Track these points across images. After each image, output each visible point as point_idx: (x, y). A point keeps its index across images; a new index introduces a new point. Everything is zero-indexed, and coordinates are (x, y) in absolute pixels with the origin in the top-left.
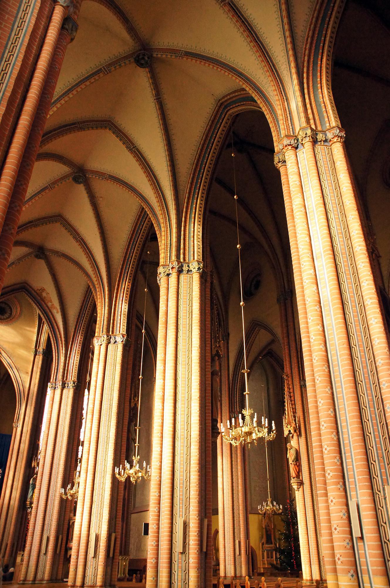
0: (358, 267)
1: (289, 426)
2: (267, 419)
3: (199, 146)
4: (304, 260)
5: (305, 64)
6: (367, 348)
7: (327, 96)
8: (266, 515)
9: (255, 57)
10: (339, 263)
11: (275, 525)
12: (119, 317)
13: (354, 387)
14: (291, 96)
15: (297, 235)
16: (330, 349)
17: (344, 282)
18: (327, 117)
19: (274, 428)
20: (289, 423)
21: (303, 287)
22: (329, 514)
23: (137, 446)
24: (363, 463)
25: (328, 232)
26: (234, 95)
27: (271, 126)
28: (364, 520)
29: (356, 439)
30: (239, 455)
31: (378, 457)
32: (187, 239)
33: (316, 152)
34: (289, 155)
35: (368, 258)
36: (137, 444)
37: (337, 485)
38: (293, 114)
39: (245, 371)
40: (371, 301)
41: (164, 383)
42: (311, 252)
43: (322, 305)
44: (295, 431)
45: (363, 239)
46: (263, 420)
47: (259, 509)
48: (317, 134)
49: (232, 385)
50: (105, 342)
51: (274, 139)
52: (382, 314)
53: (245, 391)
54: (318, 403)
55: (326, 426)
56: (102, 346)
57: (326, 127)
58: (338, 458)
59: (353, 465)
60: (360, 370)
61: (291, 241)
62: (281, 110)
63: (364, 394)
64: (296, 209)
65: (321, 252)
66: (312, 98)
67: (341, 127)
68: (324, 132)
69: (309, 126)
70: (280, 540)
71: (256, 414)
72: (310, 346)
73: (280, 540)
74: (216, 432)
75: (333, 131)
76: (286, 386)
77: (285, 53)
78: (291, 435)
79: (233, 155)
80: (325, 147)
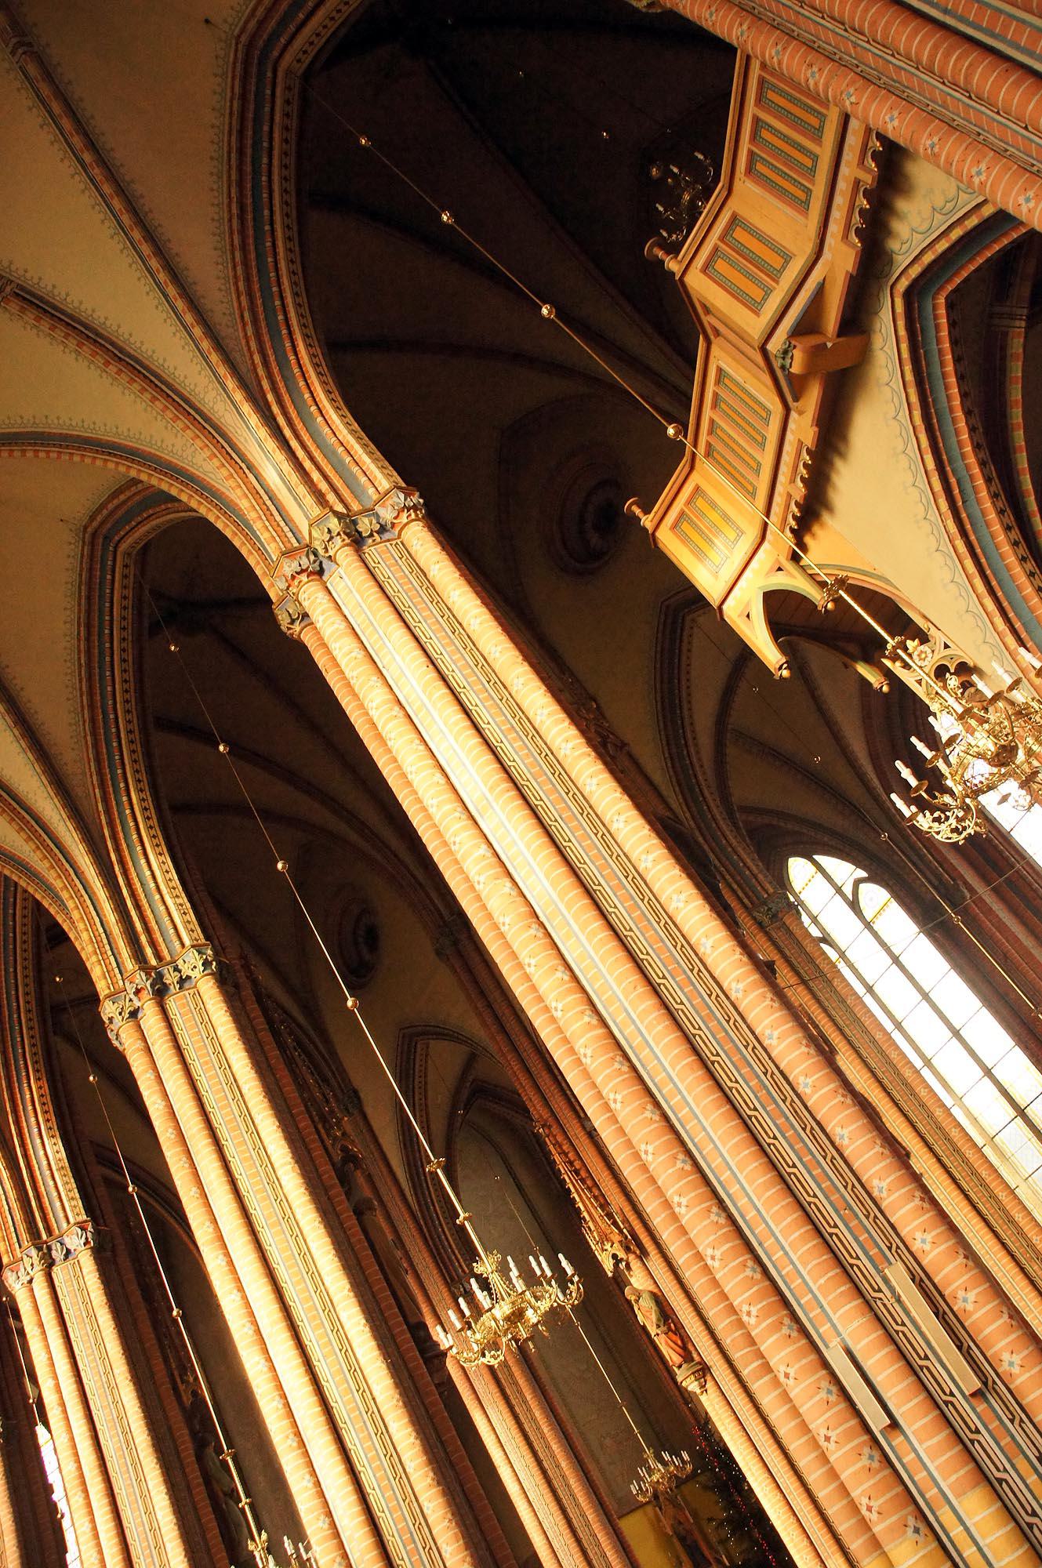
1: (608, 1246)
2: (542, 1259)
3: (79, 658)
5: (261, 371)
7: (341, 427)
8: (661, 1499)
9: (132, 396)
11: (695, 1515)
12: (51, 1183)
13: (707, 1077)
14: (257, 456)
15: (410, 777)
16: (609, 1014)
17: (570, 841)
19: (569, 1270)
20: (604, 1238)
21: (478, 898)
22: (795, 1412)
23: (247, 1507)
24: (810, 1245)
26: (116, 502)
27: (237, 543)
28: (878, 1380)
30: (521, 1381)
31: (837, 1211)
32: (144, 901)
33: (372, 564)
34: (311, 596)
36: (244, 1501)
37: (780, 1330)
39: (435, 1166)
40: (651, 857)
41: (245, 1298)
42: (460, 804)
43: (542, 918)
44: (628, 1250)
45: (567, 722)
46: (534, 1264)
47: (635, 1492)
48: (355, 523)
49: (421, 1210)
50: (38, 1267)
51: (258, 572)
52: (690, 876)
53: (458, 1216)
54: (643, 1156)
55: (687, 1202)
56: (34, 1284)
57: (369, 497)
58: (750, 1263)
59: (792, 1263)
60: (700, 1029)
61: (404, 799)
62: (247, 497)
63: (737, 1082)
66: (309, 443)
67: (404, 485)
70: (723, 1542)
71: (509, 1258)
72: (559, 1030)
73: (723, 1542)
74: (435, 1357)
75: (390, 502)
76: (553, 1151)
78: (622, 1265)
79: (173, 648)
80: (388, 544)
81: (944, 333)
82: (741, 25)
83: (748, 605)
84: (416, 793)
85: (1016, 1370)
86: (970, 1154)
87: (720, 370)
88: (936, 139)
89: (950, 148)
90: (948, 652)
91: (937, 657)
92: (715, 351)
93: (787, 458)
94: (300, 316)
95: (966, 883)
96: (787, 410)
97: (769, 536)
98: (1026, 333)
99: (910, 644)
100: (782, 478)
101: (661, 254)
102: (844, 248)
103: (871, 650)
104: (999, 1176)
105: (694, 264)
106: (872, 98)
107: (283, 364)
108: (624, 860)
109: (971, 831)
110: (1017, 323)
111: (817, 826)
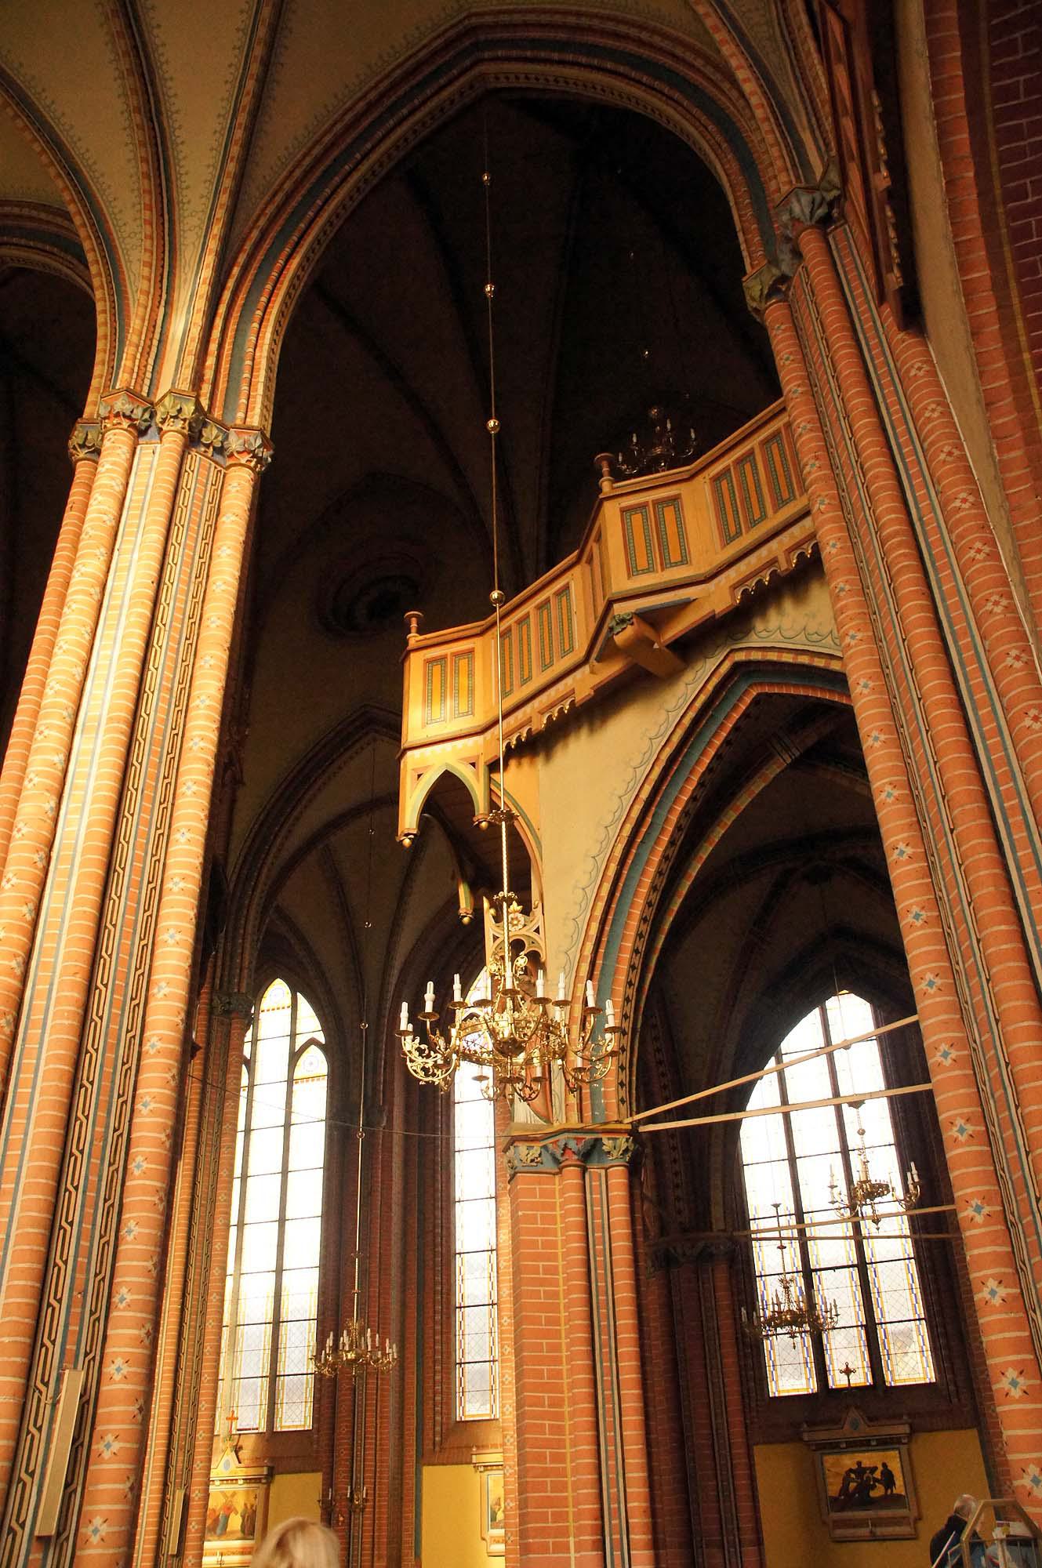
0: (181, 790)
4: (48, 721)
5: (248, 246)
6: (132, 999)
7: (266, 347)
10: (135, 762)
14: (181, 304)
15: (56, 650)
16: (35, 975)
17: (132, 815)
18: (246, 396)
25: (138, 675)
26: (34, 213)
27: (100, 345)
29: (29, 1233)
31: (71, 1289)
34: (116, 443)
35: (212, 777)
38: (168, 348)
40: (182, 885)
43: (54, 855)
45: (216, 725)
48: (205, 425)
51: (95, 382)
52: (198, 926)
57: (235, 418)
62: (143, 321)
64: (78, 583)
65: (101, 716)
66: (230, 333)
67: (268, 435)
68: (224, 428)
69: (194, 394)
77: (214, 176)
80: (213, 465)
81: (736, 716)
82: (799, 386)
83: (427, 768)
84: (49, 666)
85: (95, 1540)
86: (210, 1324)
87: (567, 587)
88: (847, 587)
89: (850, 602)
90: (534, 935)
91: (524, 931)
92: (577, 570)
93: (553, 693)
94: (318, 241)
95: (391, 1112)
96: (586, 661)
97: (488, 734)
98: (786, 768)
99: (515, 906)
100: (537, 703)
101: (605, 469)
102: (727, 592)
103: (485, 883)
104: (218, 1361)
105: (620, 500)
106: (833, 520)
107: (270, 258)
108: (160, 868)
109: (436, 1080)
110: (786, 757)
111: (322, 975)
